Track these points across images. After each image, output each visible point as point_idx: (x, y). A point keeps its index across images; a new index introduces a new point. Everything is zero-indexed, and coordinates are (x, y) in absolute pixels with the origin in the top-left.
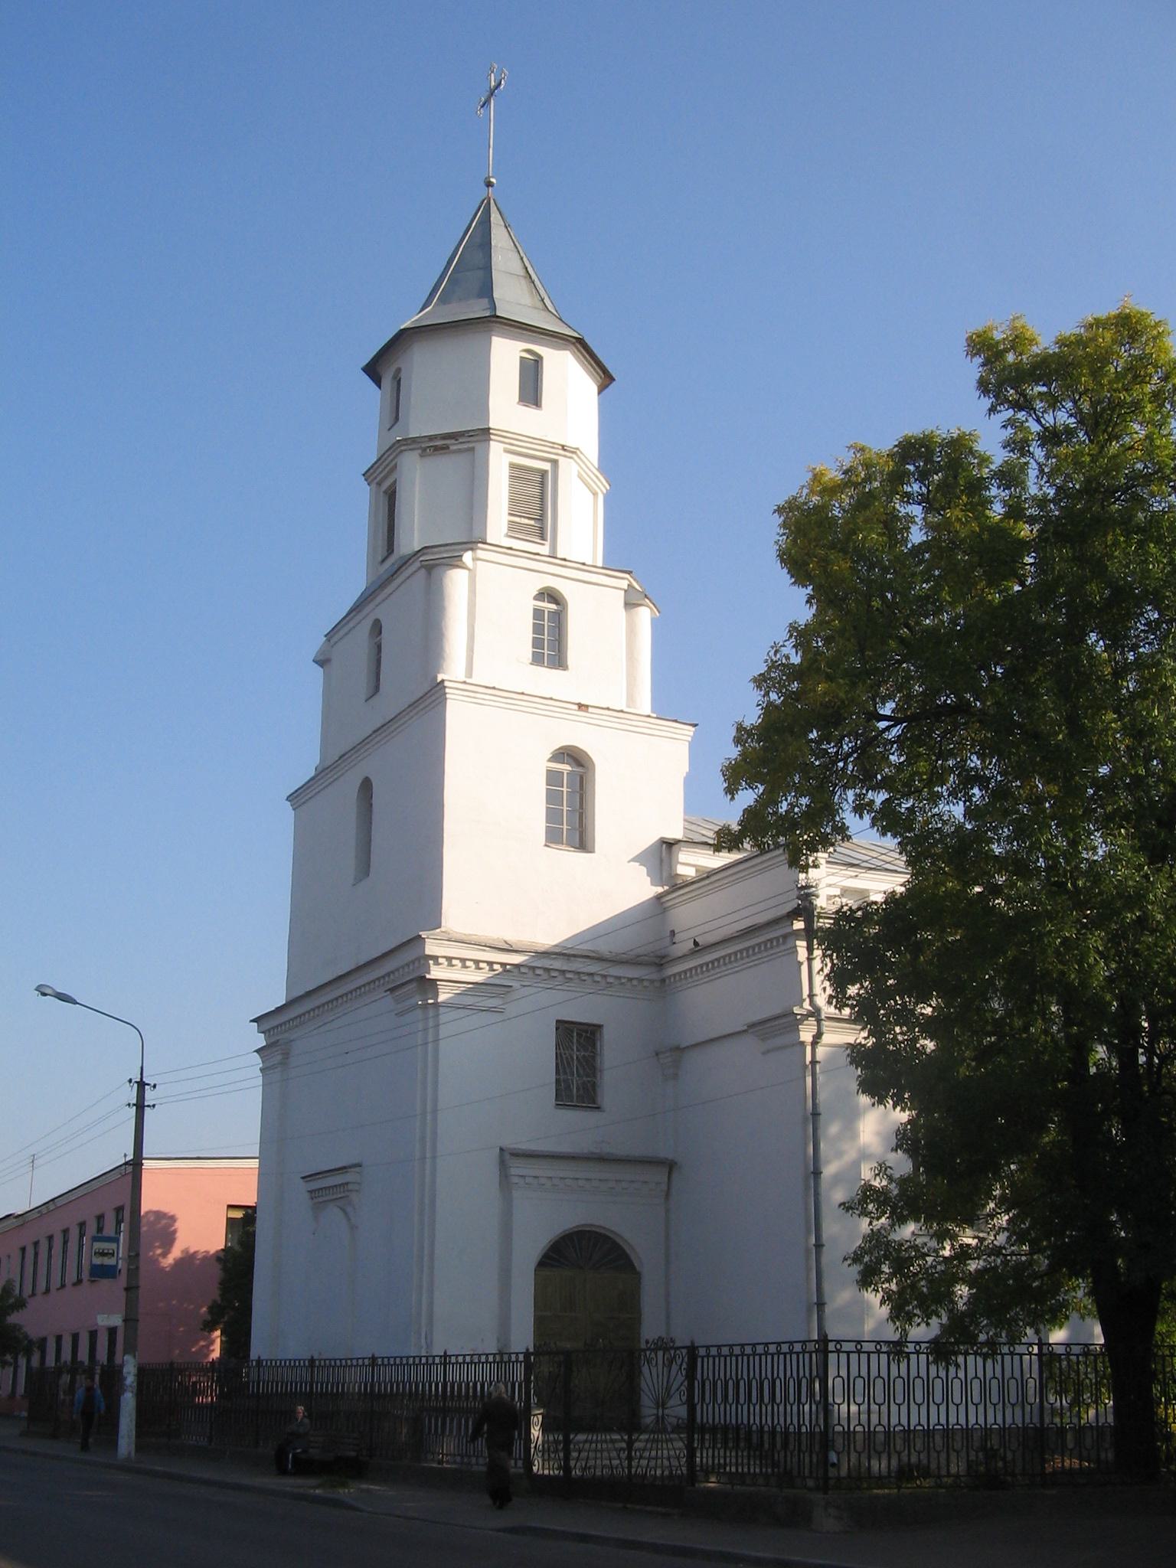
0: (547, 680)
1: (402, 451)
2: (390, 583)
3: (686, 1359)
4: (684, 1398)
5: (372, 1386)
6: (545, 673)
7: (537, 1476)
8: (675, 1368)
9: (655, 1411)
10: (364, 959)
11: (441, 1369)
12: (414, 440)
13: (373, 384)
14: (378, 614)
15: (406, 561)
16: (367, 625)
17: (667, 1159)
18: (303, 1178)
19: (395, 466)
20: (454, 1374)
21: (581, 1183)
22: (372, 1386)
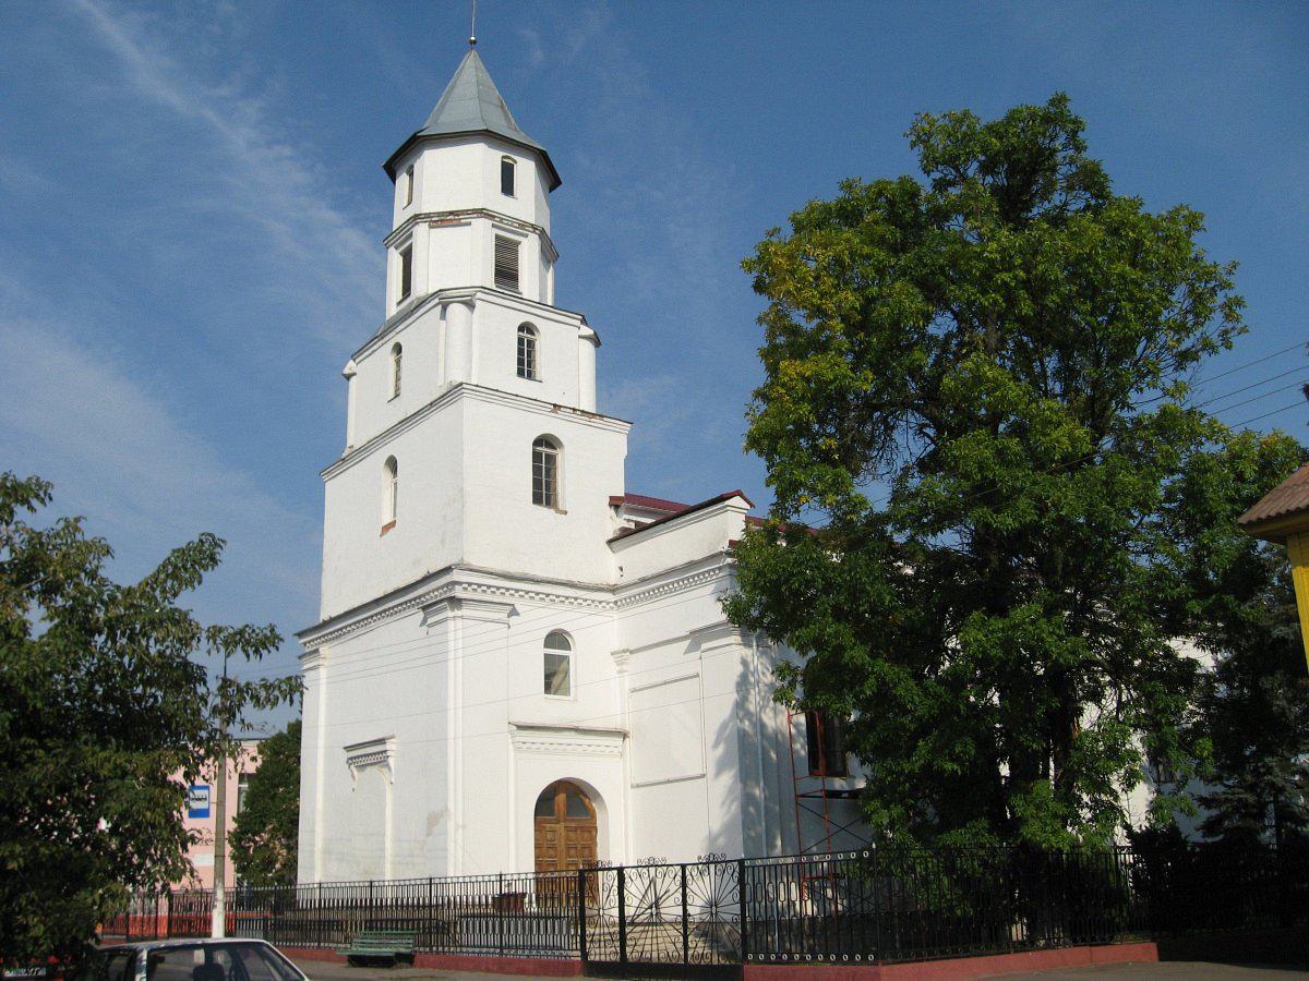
0: (523, 386)
1: (417, 223)
2: (410, 317)
3: (737, 870)
4: (737, 899)
5: (371, 900)
6: (524, 382)
7: (593, 962)
8: (727, 876)
9: (709, 910)
10: (575, 579)
11: (318, 891)
12: (428, 215)
13: (387, 177)
14: (399, 338)
15: (422, 302)
16: (391, 345)
17: (724, 721)
18: (345, 748)
19: (411, 235)
20: (326, 894)
21: (555, 746)
22: (371, 900)
